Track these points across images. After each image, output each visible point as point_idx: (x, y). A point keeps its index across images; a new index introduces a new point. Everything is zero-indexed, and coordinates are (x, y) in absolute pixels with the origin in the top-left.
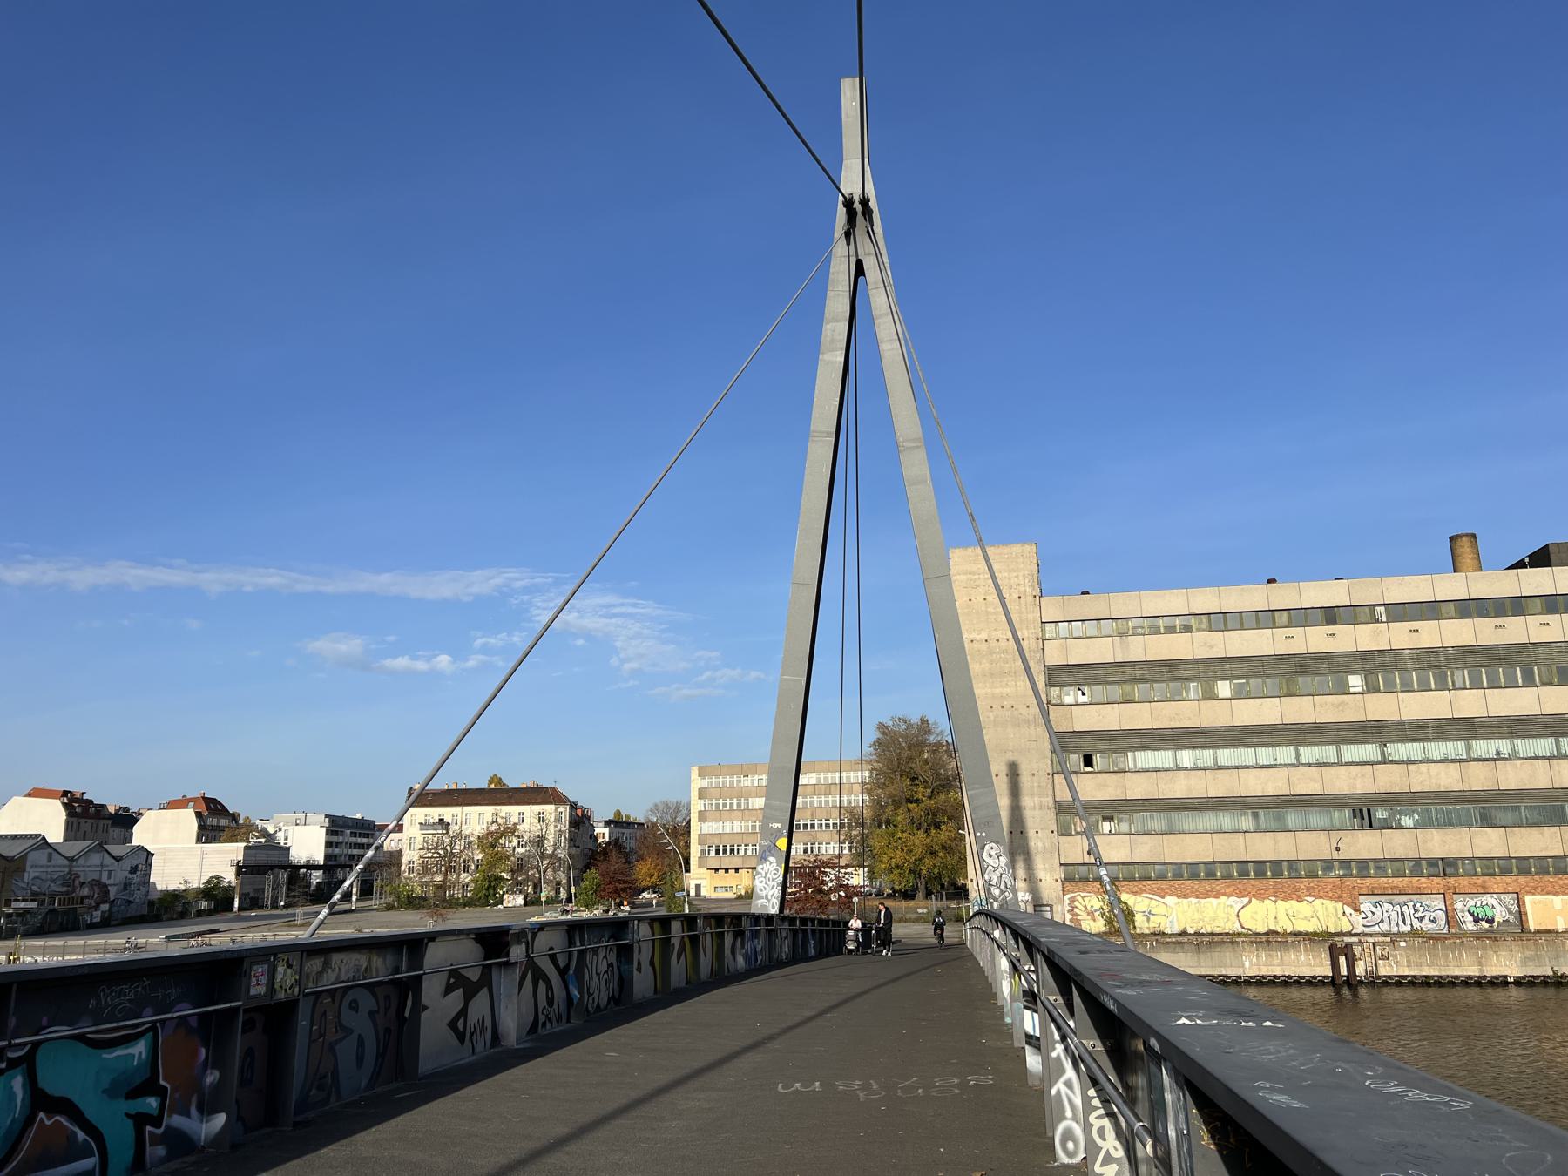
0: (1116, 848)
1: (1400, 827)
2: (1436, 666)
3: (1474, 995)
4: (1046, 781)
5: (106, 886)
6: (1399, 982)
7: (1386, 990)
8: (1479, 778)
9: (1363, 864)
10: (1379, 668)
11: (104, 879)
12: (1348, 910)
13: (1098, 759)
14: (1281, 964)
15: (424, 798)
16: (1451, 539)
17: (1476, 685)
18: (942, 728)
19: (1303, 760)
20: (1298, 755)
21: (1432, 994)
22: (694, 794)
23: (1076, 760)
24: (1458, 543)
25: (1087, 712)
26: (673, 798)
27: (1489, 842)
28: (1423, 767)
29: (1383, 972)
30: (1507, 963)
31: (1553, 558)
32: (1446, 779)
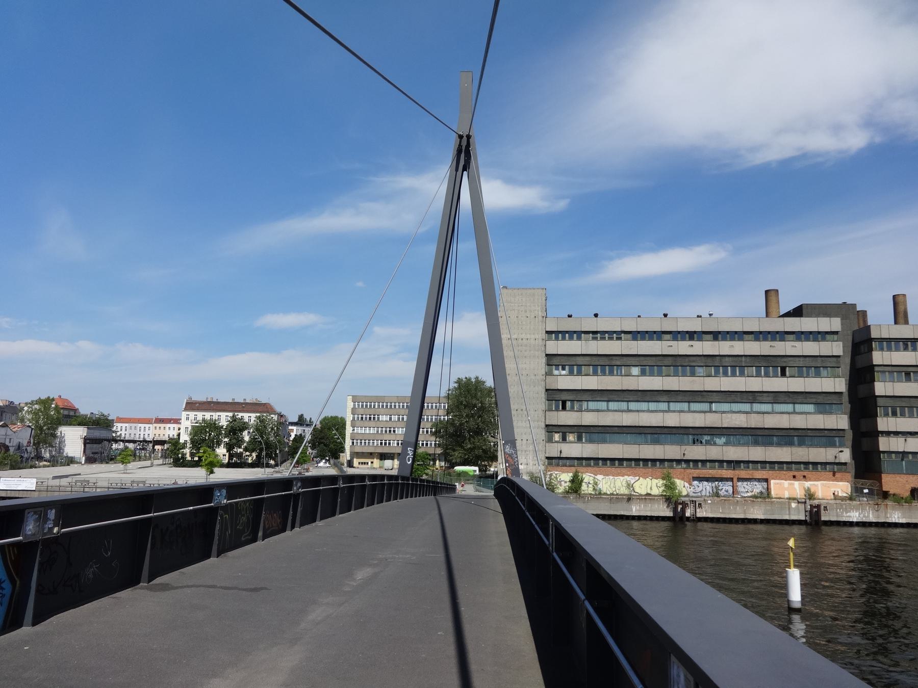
0: (573, 449)
1: (715, 444)
2: (738, 365)
3: (741, 527)
4: (541, 414)
5: (8, 447)
6: (706, 520)
7: (699, 524)
8: (754, 421)
9: (696, 462)
10: (716, 364)
11: (7, 443)
12: (687, 485)
13: (568, 404)
14: (651, 511)
15: (191, 406)
16: (767, 292)
17: (758, 375)
18: (490, 383)
19: (672, 409)
20: (711, 408)
21: (722, 526)
22: (349, 411)
23: (557, 437)
24: (769, 294)
25: (565, 381)
26: (329, 413)
27: (757, 453)
28: (729, 415)
29: (699, 515)
30: (757, 513)
31: (804, 312)
32: (739, 421)
